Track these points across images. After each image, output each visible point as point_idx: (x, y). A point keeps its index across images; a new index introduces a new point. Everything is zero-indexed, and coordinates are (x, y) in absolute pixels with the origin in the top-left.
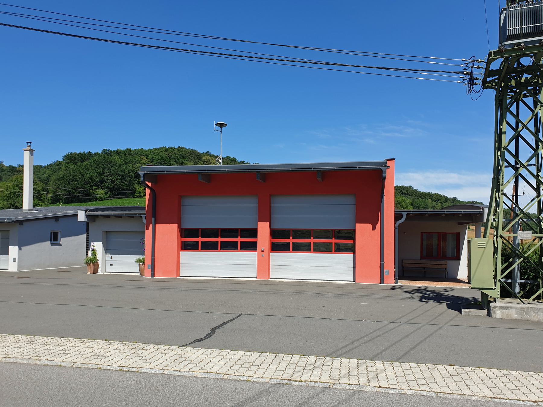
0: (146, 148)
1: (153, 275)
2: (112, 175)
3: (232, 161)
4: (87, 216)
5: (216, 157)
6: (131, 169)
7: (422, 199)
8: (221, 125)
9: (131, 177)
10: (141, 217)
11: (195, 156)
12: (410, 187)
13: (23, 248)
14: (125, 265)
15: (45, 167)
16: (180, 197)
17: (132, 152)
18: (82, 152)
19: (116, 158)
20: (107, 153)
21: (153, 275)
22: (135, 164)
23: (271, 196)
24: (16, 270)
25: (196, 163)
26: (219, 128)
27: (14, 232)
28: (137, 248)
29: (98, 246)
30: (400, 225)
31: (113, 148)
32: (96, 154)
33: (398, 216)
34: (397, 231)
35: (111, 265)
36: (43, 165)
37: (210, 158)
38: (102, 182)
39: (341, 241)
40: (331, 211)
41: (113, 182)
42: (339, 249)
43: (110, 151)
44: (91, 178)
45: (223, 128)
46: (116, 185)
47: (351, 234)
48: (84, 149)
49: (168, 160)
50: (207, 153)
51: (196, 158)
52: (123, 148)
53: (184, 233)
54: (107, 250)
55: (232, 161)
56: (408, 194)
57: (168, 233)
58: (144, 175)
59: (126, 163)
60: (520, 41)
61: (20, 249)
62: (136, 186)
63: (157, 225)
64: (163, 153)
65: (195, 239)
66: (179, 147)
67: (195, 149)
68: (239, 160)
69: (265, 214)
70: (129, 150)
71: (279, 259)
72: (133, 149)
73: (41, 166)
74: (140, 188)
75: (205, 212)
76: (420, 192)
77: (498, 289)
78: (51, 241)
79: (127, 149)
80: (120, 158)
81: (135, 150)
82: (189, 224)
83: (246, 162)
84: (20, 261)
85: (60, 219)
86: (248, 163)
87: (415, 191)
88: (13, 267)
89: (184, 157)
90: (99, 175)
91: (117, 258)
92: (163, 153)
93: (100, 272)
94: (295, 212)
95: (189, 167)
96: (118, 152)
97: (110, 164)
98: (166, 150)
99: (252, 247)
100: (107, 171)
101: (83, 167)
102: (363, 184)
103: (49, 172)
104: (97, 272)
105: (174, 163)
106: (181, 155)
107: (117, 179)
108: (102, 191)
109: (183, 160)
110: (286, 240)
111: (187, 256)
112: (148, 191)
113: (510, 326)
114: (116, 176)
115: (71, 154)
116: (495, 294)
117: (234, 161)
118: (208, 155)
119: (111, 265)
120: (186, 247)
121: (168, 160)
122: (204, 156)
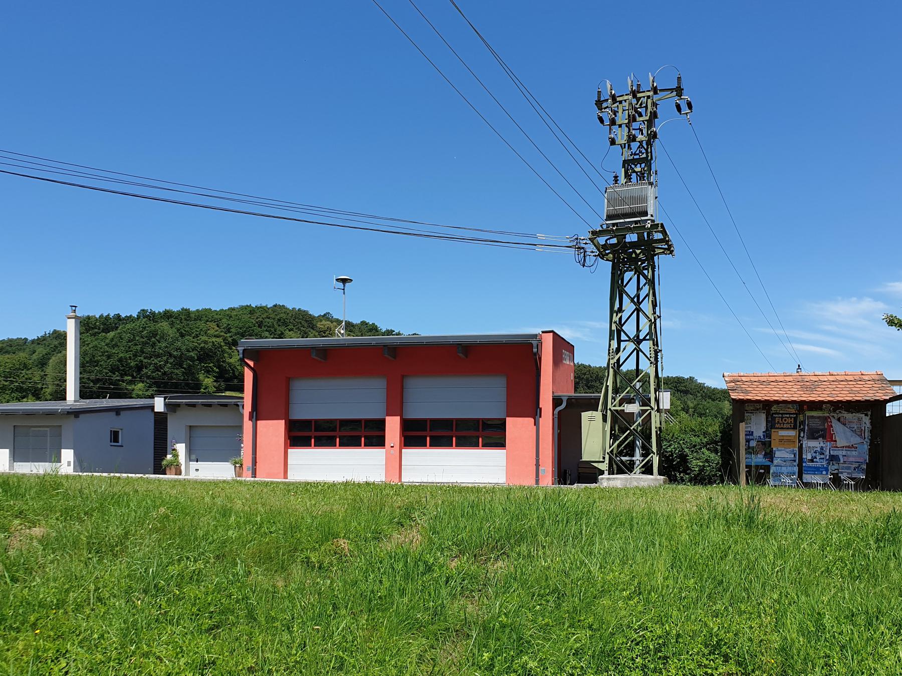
0: (216, 307)
1: (254, 475)
2: (158, 356)
3: (371, 330)
4: (166, 405)
5: (339, 322)
6: (191, 345)
7: (713, 400)
8: (344, 281)
9: (192, 359)
10: (238, 405)
11: (303, 321)
12: (691, 379)
15: (33, 341)
16: (288, 381)
17: (193, 316)
18: (105, 315)
19: (164, 325)
20: (148, 316)
21: (254, 475)
22: (197, 336)
23: (403, 377)
25: (305, 335)
26: (341, 285)
28: (227, 451)
30: (560, 412)
31: (158, 308)
32: (129, 319)
33: (557, 402)
34: (556, 420)
35: (197, 470)
36: (30, 339)
37: (332, 325)
38: (139, 368)
39: (486, 433)
40: (479, 397)
41: (157, 368)
43: (153, 313)
44: (120, 360)
45: (347, 284)
46: (165, 373)
47: (501, 426)
48: (111, 311)
49: (257, 329)
50: (326, 317)
51: (306, 325)
52: (176, 308)
54: (190, 451)
55: (371, 330)
56: (686, 392)
58: (244, 350)
59: (182, 335)
60: (639, 219)
62: (201, 377)
64: (246, 317)
66: (275, 306)
67: (302, 308)
68: (383, 328)
69: (395, 405)
70: (186, 313)
71: (412, 455)
72: (193, 309)
73: (26, 339)
74: (206, 380)
76: (709, 388)
77: (607, 461)
79: (183, 309)
80: (172, 325)
81: (198, 310)
82: (300, 413)
83: (397, 331)
85: (122, 413)
86: (399, 334)
87: (701, 387)
89: (285, 324)
90: (135, 355)
91: (200, 465)
92: (246, 317)
94: (432, 399)
95: (293, 340)
96: (168, 315)
98: (251, 311)
99: (378, 441)
100: (148, 349)
101: (107, 341)
102: (512, 362)
103: (41, 350)
105: (267, 334)
106: (279, 320)
107: (167, 362)
108: (140, 385)
109: (282, 329)
110: (418, 434)
111: (298, 455)
114: (165, 358)
115: (89, 318)
116: (604, 467)
117: (373, 329)
118: (328, 319)
119: (197, 470)
121: (257, 329)
122: (321, 321)
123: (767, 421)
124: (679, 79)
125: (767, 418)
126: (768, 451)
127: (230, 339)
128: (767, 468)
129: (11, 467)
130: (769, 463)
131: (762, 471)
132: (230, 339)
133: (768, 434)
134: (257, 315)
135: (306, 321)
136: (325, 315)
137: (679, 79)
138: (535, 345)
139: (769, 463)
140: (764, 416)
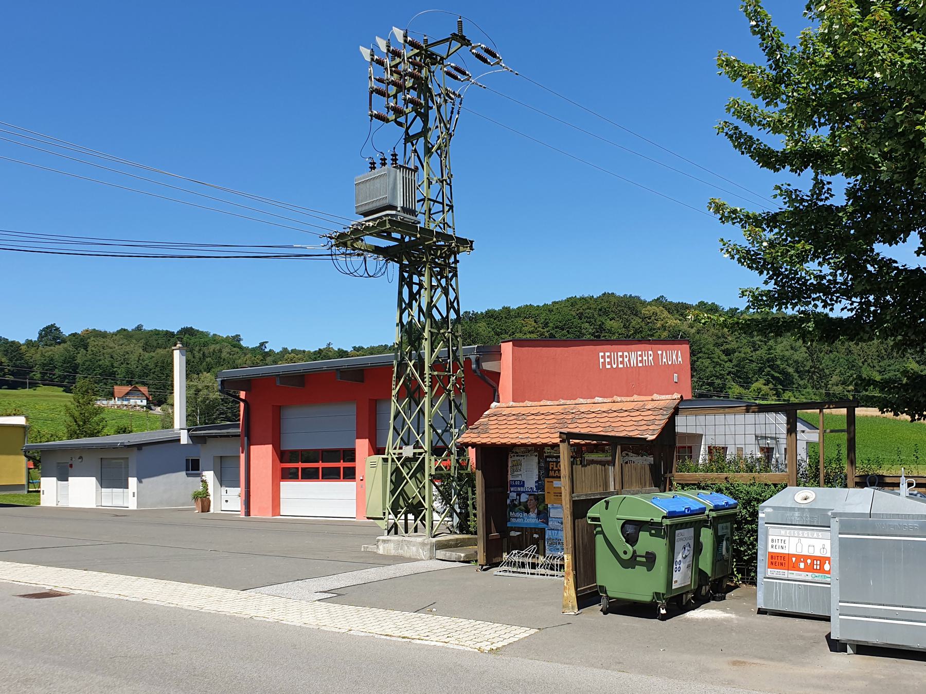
4: (191, 437)
13: (143, 480)
14: (227, 500)
24: (94, 506)
27: (134, 458)
29: (209, 476)
42: (331, 475)
52: (498, 308)
53: (282, 455)
57: (262, 456)
58: (222, 381)
61: (140, 481)
63: (252, 447)
65: (300, 464)
70: (507, 310)
72: (514, 306)
75: (309, 427)
78: (187, 470)
79: (504, 308)
82: (291, 443)
84: (139, 495)
88: (132, 504)
89: (606, 313)
93: (212, 510)
97: (470, 336)
104: (208, 511)
106: (600, 310)
111: (288, 488)
112: (242, 404)
113: (361, 560)
120: (289, 475)
123: (540, 468)
124: (460, 23)
125: (539, 463)
126: (541, 508)
127: (547, 334)
128: (542, 532)
129: (99, 496)
130: (543, 526)
131: (536, 536)
132: (547, 334)
133: (540, 486)
134: (577, 307)
135: (630, 308)
136: (658, 299)
137: (460, 23)
138: (473, 360)
139: (543, 526)
140: (536, 459)
